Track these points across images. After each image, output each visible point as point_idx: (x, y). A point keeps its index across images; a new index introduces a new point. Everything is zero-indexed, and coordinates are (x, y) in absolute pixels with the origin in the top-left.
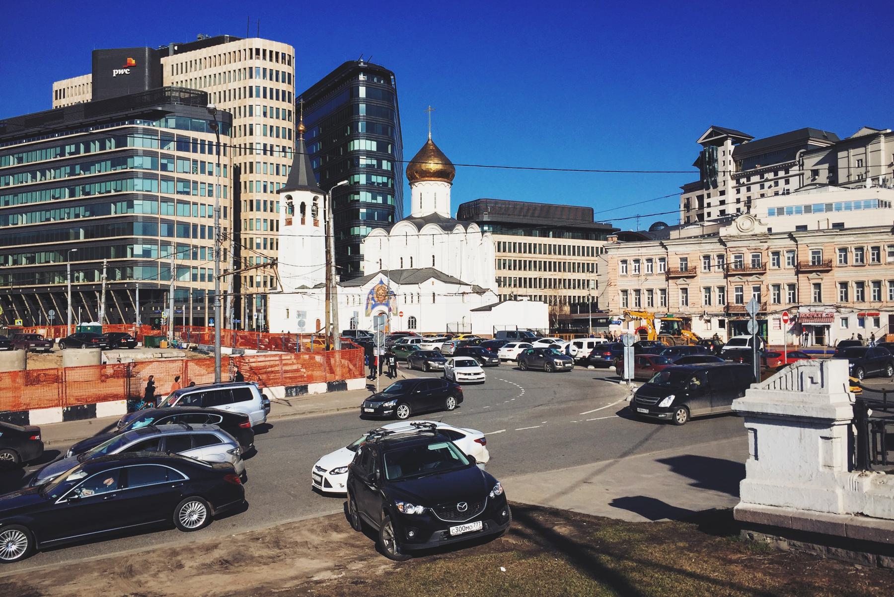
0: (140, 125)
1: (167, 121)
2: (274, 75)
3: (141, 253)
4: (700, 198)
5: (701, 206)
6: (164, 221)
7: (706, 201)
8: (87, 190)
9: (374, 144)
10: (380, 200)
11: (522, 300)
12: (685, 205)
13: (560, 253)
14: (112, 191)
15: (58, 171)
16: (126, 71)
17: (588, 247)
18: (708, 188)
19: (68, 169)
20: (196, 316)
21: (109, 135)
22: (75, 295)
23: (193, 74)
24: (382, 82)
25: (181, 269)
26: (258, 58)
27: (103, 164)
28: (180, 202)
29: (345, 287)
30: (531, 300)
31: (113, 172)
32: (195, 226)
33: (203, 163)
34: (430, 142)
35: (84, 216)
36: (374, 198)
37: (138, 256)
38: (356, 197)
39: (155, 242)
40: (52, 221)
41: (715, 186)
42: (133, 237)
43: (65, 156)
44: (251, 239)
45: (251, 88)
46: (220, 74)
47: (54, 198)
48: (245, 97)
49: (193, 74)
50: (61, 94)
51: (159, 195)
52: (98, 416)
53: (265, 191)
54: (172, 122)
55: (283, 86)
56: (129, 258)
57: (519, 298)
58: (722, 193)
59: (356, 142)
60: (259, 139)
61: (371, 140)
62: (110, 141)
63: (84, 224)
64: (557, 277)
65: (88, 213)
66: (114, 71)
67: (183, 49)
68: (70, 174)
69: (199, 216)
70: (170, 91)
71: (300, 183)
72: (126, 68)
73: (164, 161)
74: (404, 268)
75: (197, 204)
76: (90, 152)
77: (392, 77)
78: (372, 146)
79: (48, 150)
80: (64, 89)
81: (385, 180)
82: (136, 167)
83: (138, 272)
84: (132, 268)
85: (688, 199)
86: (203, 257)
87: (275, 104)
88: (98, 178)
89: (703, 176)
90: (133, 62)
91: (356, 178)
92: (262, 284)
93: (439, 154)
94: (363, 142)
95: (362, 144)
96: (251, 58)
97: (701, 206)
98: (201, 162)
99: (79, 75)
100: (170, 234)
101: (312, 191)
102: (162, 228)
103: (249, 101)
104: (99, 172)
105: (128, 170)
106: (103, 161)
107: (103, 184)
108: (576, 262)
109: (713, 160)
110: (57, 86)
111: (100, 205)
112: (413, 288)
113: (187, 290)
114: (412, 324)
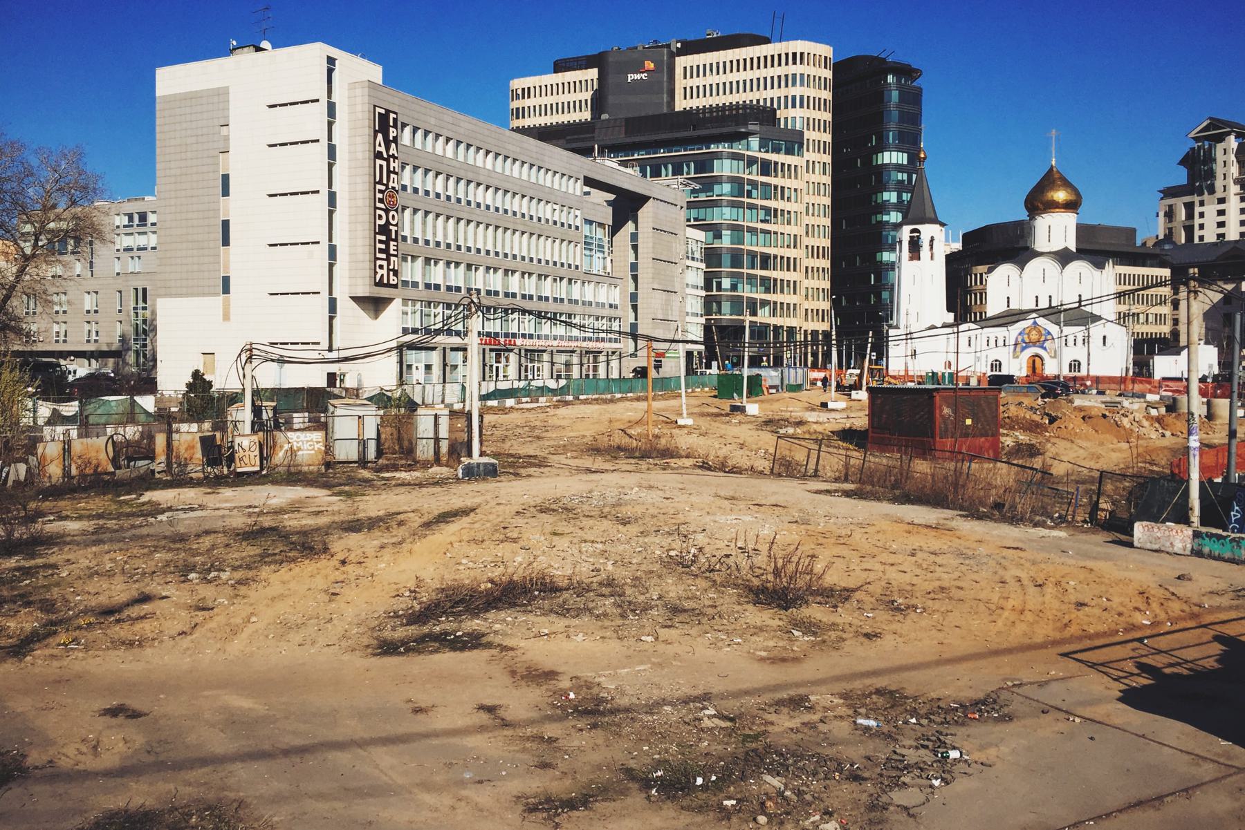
3: (729, 287)
4: (1190, 207)
5: (1190, 216)
7: (1198, 210)
12: (1165, 213)
16: (643, 76)
18: (1201, 194)
25: (764, 303)
37: (726, 290)
38: (885, 218)
41: (1212, 191)
51: (745, 224)
54: (754, 142)
58: (1222, 201)
59: (887, 154)
73: (750, 188)
74: (1039, 307)
85: (1170, 206)
89: (1192, 177)
91: (886, 196)
93: (1067, 184)
97: (1190, 216)
105: (715, 198)
109: (1210, 159)
110: (517, 84)
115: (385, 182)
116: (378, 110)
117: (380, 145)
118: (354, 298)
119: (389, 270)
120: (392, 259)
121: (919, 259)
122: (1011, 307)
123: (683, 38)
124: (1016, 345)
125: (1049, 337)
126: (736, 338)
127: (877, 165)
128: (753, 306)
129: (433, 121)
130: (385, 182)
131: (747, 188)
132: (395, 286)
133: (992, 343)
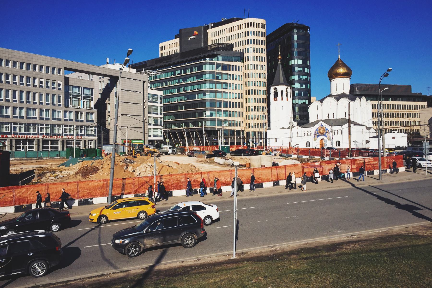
0: (208, 60)
1: (218, 58)
6: (218, 101)
8: (185, 89)
9: (301, 61)
10: (304, 87)
11: (394, 132)
13: (395, 109)
14: (197, 89)
15: (172, 82)
16: (194, 37)
17: (410, 105)
19: (177, 81)
20: (231, 141)
21: (194, 66)
22: (188, 134)
23: (221, 36)
24: (304, 32)
25: (226, 121)
26: (251, 27)
27: (192, 78)
28: (224, 92)
29: (303, 128)
30: (398, 132)
32: (230, 102)
33: (233, 75)
34: (339, 60)
35: (184, 100)
36: (302, 86)
37: (208, 116)
39: (214, 110)
40: (170, 103)
42: (206, 108)
43: (175, 75)
44: (249, 107)
45: (248, 40)
46: (234, 35)
47: (171, 93)
48: (245, 44)
49: (221, 36)
50: (163, 48)
51: (216, 90)
52: (374, 174)
53: (255, 85)
57: (393, 131)
59: (293, 61)
60: (251, 62)
61: (300, 59)
62: (195, 68)
63: (184, 104)
64: (395, 121)
66: (189, 37)
67: (215, 25)
69: (232, 98)
70: (218, 45)
71: (281, 82)
72: (194, 36)
73: (218, 75)
74: (330, 119)
75: (230, 93)
76: (186, 73)
77: (308, 29)
78: (300, 62)
79: (168, 73)
80: (164, 46)
81: (306, 77)
82: (207, 79)
83: (208, 123)
86: (234, 116)
88: (190, 84)
91: (293, 77)
92: (254, 127)
94: (296, 60)
95: (296, 62)
96: (248, 27)
98: (232, 75)
99: (171, 40)
100: (220, 107)
101: (286, 85)
102: (217, 104)
103: (247, 46)
104: (191, 81)
105: (203, 80)
107: (192, 87)
108: (404, 112)
110: (161, 45)
111: (192, 95)
112: (339, 128)
113: (227, 130)
114: (338, 144)
121: (277, 100)
122: (319, 119)
124: (315, 135)
125: (327, 131)
126: (215, 135)
127: (292, 65)
128: (220, 122)
133: (306, 134)
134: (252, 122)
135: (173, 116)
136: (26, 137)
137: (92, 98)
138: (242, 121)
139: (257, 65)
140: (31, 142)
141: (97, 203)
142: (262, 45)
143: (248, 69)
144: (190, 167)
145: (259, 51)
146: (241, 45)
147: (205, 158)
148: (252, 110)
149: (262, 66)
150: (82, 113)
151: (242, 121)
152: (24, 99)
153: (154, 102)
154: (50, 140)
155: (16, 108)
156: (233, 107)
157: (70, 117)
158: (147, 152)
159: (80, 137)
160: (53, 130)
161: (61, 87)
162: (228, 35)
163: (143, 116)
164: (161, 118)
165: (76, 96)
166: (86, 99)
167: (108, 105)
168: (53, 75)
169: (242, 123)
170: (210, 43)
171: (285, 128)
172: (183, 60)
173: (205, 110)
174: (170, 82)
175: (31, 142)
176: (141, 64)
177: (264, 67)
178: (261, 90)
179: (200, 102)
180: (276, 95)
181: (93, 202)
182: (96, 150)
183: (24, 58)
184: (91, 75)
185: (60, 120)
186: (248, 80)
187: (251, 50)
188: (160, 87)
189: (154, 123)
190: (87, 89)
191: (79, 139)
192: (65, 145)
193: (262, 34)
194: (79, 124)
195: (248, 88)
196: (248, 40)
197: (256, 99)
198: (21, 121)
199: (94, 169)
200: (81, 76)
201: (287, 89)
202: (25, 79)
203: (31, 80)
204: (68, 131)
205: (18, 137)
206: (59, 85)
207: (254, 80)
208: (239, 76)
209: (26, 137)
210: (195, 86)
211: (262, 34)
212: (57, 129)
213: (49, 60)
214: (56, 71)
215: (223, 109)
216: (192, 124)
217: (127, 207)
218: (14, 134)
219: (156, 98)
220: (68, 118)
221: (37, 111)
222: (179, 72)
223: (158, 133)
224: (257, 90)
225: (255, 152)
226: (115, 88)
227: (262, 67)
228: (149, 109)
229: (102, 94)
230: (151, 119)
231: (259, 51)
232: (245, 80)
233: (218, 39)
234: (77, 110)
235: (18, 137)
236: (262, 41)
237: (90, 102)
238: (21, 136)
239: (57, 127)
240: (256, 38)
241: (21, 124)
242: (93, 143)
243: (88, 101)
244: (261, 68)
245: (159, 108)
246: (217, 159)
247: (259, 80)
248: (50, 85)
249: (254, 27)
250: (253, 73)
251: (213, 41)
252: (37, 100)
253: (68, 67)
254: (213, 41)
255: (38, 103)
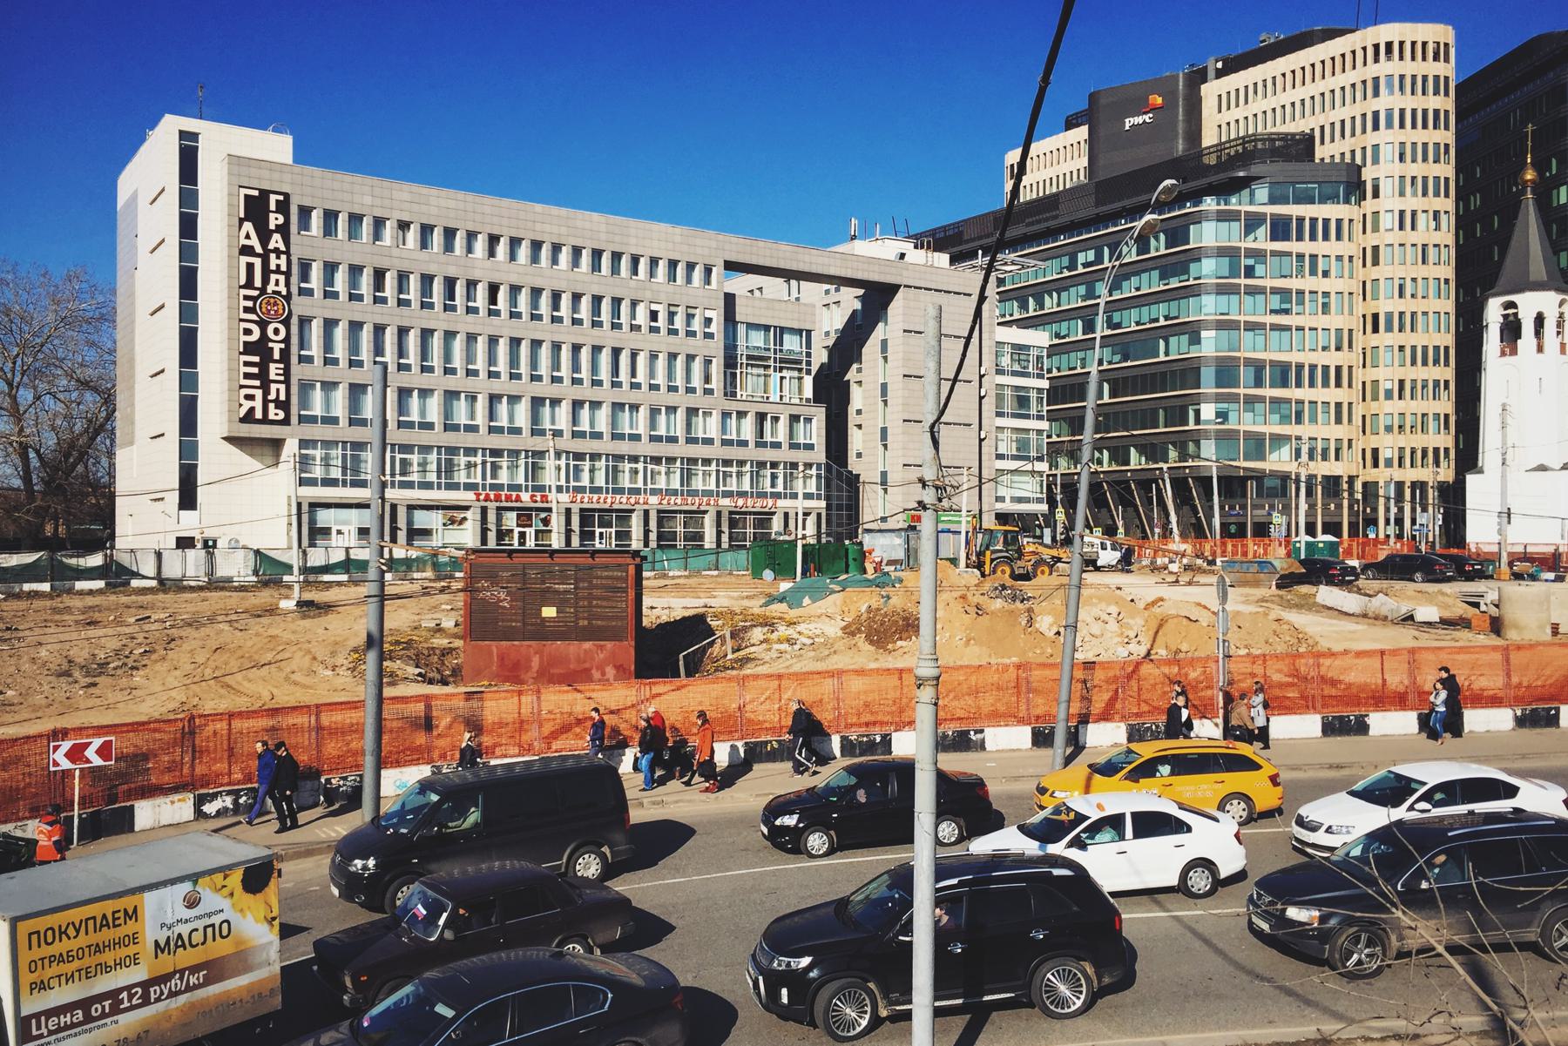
0: (1210, 204)
1: (1252, 194)
2: (1418, 85)
3: (1213, 416)
14: (1162, 319)
15: (1064, 295)
16: (1147, 118)
19: (1082, 290)
20: (1328, 519)
23: (1258, 105)
25: (1278, 440)
27: (1145, 276)
31: (1162, 288)
33: (1314, 257)
35: (1110, 363)
37: (1208, 422)
39: (1234, 398)
45: (1376, 114)
48: (1364, 131)
49: (1258, 105)
51: (1242, 318)
54: (1262, 193)
55: (1434, 102)
56: (1191, 426)
60: (1389, 203)
62: (1157, 239)
65: (1117, 358)
67: (1232, 66)
68: (1085, 298)
69: (1307, 348)
72: (1145, 113)
73: (1251, 262)
75: (1302, 329)
83: (1208, 449)
84: (1197, 443)
86: (1314, 420)
87: (1420, 136)
90: (1159, 100)
96: (1376, 60)
100: (1259, 383)
101: (1558, 290)
102: (1245, 374)
103: (1371, 138)
105: (1191, 282)
106: (1144, 271)
107: (1145, 310)
111: (1148, 339)
115: (258, 283)
116: (244, 191)
117: (248, 237)
118: (224, 438)
119: (266, 402)
120: (273, 387)
123: (1226, 54)
128: (1258, 444)
129: (368, 200)
130: (258, 283)
131: (1245, 262)
132: (286, 422)
134: (1388, 445)
135: (1063, 424)
136: (609, 500)
137: (809, 363)
138: (1350, 441)
139: (1414, 213)
140: (624, 515)
141: (1000, 748)
142: (1435, 127)
143: (1376, 229)
144: (1275, 626)
145: (1423, 153)
146: (1343, 136)
147: (1274, 587)
148: (1389, 395)
149: (1436, 214)
150: (776, 419)
151: (1350, 441)
152: (604, 374)
153: (1015, 374)
154: (681, 512)
155: (500, 397)
156: (1312, 385)
157: (592, 424)
158: (1034, 559)
159: (770, 502)
160: (687, 476)
161: (713, 329)
162: (1286, 98)
163: (976, 426)
164: (1039, 432)
165: (756, 360)
166: (788, 368)
167: (854, 388)
168: (689, 290)
169: (1350, 446)
170: (1209, 139)
171: (1552, 470)
172: (1104, 208)
173: (1197, 400)
174: (1055, 294)
175: (624, 515)
176: (942, 235)
177: (1444, 218)
178: (1431, 314)
179: (1175, 367)
180: (1511, 330)
181: (983, 741)
182: (847, 550)
183: (603, 236)
184: (794, 283)
185: (635, 438)
186: (1374, 273)
187: (1388, 153)
188: (1017, 316)
189: (1015, 453)
190: (793, 331)
191: (766, 510)
192: (725, 528)
193: (1440, 86)
194: (768, 455)
195: (1371, 307)
196: (1376, 114)
197: (1408, 351)
198: (424, 437)
199: (905, 619)
200: (760, 289)
201: (1561, 305)
202: (606, 306)
203: (625, 308)
204: (415, 468)
205: (586, 500)
206: (708, 321)
207: (1399, 272)
208: (1339, 258)
209: (609, 500)
210: (1154, 307)
211: (1440, 86)
212: (700, 473)
213: (678, 239)
214: (698, 274)
215: (1268, 392)
216: (1142, 450)
217: (1179, 774)
218: (493, 487)
219: (1022, 357)
220: (734, 437)
221: (643, 413)
222: (1091, 255)
223: (1030, 487)
224: (1413, 314)
225: (1473, 565)
226: (881, 325)
227: (1435, 219)
228: (1000, 398)
229: (832, 351)
230: (1007, 434)
231: (1423, 153)
232: (1361, 273)
233: (1246, 118)
234: (763, 408)
235: (586, 500)
236: (1436, 112)
237: (800, 379)
238: (595, 497)
239: (700, 467)
240: (1409, 102)
241: (595, 457)
242: (811, 520)
243: (796, 374)
244: (1433, 224)
245: (1033, 395)
246: (1327, 594)
247: (1422, 271)
248: (679, 322)
249: (1401, 58)
250: (1396, 246)
251: (1224, 127)
252: (641, 377)
253: (733, 258)
254: (1224, 127)
255: (645, 387)
